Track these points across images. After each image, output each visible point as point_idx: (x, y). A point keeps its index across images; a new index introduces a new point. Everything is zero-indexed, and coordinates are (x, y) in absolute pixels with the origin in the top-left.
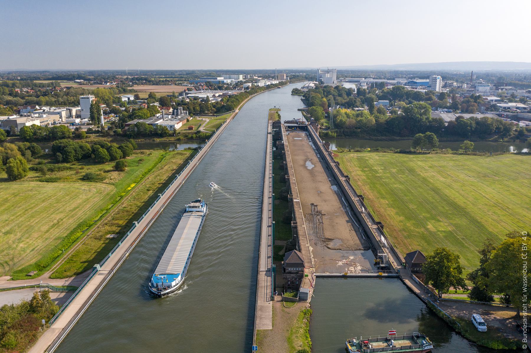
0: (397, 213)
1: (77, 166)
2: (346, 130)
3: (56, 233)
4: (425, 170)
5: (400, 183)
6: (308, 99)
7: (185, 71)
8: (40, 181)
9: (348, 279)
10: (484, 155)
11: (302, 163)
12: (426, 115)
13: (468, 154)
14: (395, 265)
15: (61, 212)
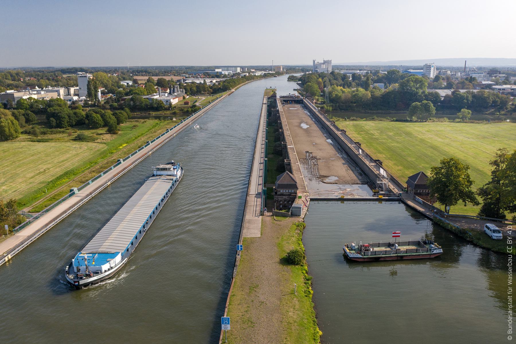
0: (395, 164)
1: (71, 130)
2: (342, 104)
3: (41, 178)
4: (422, 133)
5: (398, 142)
6: (304, 82)
7: (184, 66)
8: (32, 141)
9: (345, 202)
10: (481, 123)
11: (297, 124)
12: (422, 88)
13: (466, 122)
14: (396, 191)
15: (49, 163)
